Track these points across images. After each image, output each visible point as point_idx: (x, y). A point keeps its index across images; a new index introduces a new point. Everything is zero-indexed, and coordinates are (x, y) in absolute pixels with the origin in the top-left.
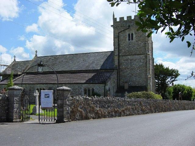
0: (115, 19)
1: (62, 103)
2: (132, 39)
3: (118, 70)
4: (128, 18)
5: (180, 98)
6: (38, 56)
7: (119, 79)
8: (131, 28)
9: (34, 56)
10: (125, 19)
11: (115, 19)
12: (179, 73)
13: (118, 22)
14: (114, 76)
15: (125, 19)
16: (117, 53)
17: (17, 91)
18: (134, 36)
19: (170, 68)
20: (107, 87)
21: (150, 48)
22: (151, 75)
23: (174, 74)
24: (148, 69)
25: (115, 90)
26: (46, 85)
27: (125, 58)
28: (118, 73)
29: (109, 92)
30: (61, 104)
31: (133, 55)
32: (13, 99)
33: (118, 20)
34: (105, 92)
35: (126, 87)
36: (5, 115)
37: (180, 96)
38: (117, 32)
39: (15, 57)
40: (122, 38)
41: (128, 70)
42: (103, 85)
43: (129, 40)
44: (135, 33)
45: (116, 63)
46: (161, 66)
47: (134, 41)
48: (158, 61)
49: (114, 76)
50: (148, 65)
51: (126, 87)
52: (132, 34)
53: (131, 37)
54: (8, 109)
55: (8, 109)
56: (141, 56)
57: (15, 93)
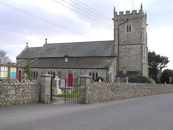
0: (115, 13)
1: (84, 88)
2: (130, 31)
3: (118, 57)
4: (127, 13)
5: (171, 82)
6: (48, 43)
7: (118, 65)
8: (130, 21)
9: (44, 43)
10: (125, 13)
11: (115, 13)
12: (168, 60)
13: (118, 16)
14: (114, 62)
15: (125, 13)
16: (116, 43)
17: (48, 78)
18: (132, 28)
19: (157, 54)
20: (109, 73)
21: (145, 38)
22: (145, 61)
23: (164, 60)
24: (143, 57)
25: (115, 74)
26: (56, 69)
27: (123, 47)
28: (118, 60)
29: (110, 76)
30: (83, 89)
31: (130, 45)
32: (45, 84)
33: (118, 14)
34: (107, 75)
35: (125, 72)
36: (38, 97)
37: (170, 81)
38: (117, 24)
39: (27, 44)
40: (121, 30)
41: (126, 57)
42: (106, 70)
43: (128, 31)
44: (133, 26)
45: (116, 51)
46: (154, 53)
47: (132, 32)
48: (151, 49)
49: (114, 62)
50: (143, 54)
51: (125, 72)
52: (130, 27)
53: (129, 29)
54: (40, 93)
55: (40, 93)
56: (138, 46)
57: (46, 79)
